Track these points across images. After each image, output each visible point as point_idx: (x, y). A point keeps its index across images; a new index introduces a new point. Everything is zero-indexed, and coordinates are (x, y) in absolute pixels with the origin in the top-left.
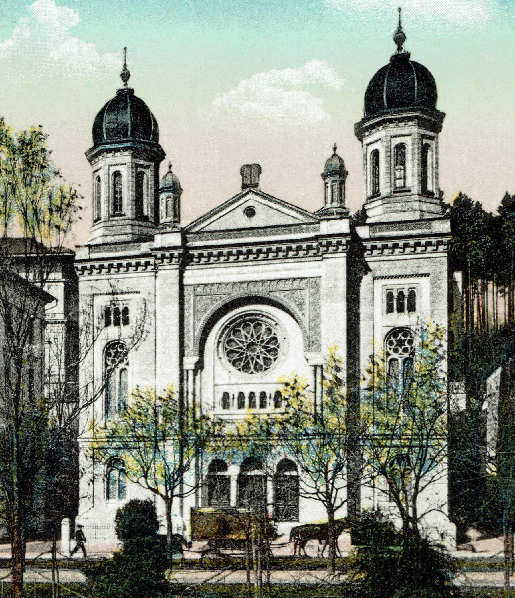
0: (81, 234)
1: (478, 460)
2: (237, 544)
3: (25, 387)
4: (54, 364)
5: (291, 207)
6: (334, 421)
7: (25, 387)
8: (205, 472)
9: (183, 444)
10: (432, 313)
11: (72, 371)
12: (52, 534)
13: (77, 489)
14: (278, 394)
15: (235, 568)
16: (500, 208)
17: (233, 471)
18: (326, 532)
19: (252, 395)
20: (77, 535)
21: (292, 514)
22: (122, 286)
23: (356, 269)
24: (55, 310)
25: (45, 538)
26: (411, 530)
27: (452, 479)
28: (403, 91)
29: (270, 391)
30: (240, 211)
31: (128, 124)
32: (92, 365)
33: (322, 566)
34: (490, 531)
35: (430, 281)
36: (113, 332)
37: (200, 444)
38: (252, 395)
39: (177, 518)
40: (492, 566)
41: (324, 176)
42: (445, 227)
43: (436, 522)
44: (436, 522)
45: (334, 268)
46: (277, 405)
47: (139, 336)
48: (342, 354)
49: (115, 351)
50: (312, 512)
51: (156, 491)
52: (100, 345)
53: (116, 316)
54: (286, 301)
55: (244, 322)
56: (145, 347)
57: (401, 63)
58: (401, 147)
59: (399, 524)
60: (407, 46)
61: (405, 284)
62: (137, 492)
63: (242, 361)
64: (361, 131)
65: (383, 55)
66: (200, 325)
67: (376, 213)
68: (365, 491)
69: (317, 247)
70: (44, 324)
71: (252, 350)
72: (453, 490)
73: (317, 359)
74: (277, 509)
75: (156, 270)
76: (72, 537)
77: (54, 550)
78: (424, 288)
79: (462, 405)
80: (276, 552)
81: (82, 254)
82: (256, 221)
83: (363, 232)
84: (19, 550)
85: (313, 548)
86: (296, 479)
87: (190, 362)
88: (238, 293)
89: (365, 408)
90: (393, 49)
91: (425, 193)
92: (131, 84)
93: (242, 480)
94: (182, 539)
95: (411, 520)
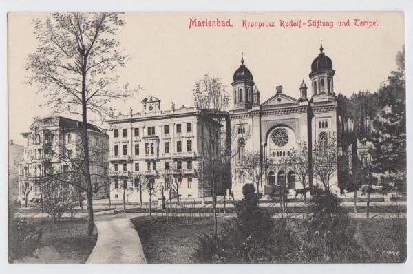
0: (230, 107)
1: (347, 170)
2: (277, 195)
3: (215, 152)
4: (223, 144)
5: (289, 97)
6: (304, 159)
7: (215, 152)
8: (268, 175)
9: (262, 167)
10: (332, 128)
11: (229, 147)
12: (224, 194)
13: (231, 181)
14: (289, 152)
15: (277, 202)
16: (342, 96)
17: (276, 175)
18: (303, 192)
19: (281, 152)
20: (231, 194)
21: (293, 186)
22: (243, 122)
23: (310, 116)
24: (224, 129)
25: (222, 195)
26: (327, 191)
27: (338, 175)
28: (322, 65)
29: (286, 151)
30: (276, 100)
31: (243, 76)
32: (234, 146)
33: (302, 201)
34: (350, 190)
35: (332, 119)
36: (240, 135)
37: (266, 167)
38: (281, 152)
39: (261, 188)
40: (350, 200)
41: (300, 89)
42: (336, 103)
43: (334, 188)
44: (334, 188)
45: (303, 116)
46: (289, 155)
47: (248, 136)
48: (306, 140)
49: (242, 141)
50: (299, 186)
51: (254, 181)
52: (237, 139)
53: (241, 130)
54: (290, 125)
55: (278, 131)
56: (250, 140)
57: (322, 56)
58: (322, 80)
59: (324, 189)
60: (323, 52)
61: (324, 120)
62: (248, 181)
63: (278, 143)
64: (311, 76)
65: (316, 54)
66: (265, 134)
67: (316, 99)
68: (314, 180)
69: (300, 109)
70: (220, 133)
71: (281, 138)
72: (339, 178)
73: (299, 142)
74: (289, 185)
75: (252, 117)
76: (230, 194)
77: (224, 198)
78: (329, 121)
79: (341, 154)
80: (289, 198)
81: (231, 113)
82: (281, 103)
83: (312, 105)
84: (215, 198)
85: (299, 196)
86: (295, 176)
87: (263, 144)
88: (276, 123)
89: (313, 156)
90: (319, 52)
91: (330, 94)
92: (323, 52)
93: (278, 177)
94: (262, 194)
95: (327, 188)
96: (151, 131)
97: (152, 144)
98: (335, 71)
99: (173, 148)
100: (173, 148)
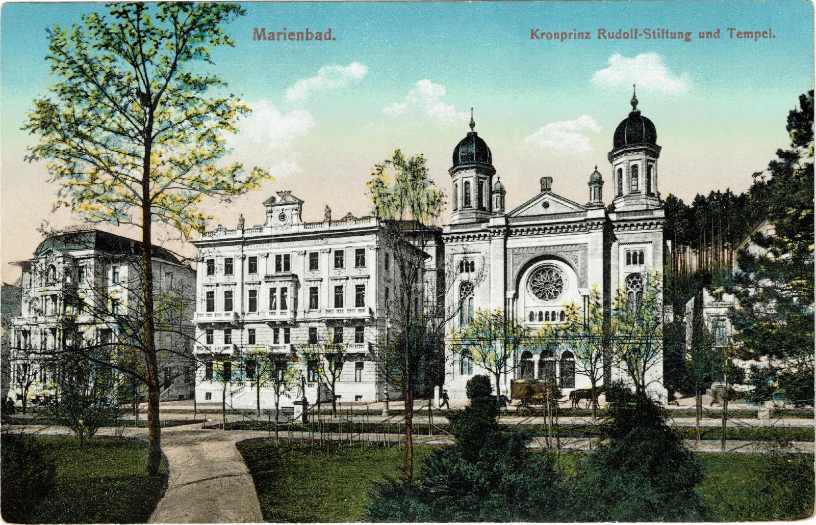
96: (283, 263)
97: (284, 290)
98: (660, 148)
99: (326, 298)
100: (326, 298)
